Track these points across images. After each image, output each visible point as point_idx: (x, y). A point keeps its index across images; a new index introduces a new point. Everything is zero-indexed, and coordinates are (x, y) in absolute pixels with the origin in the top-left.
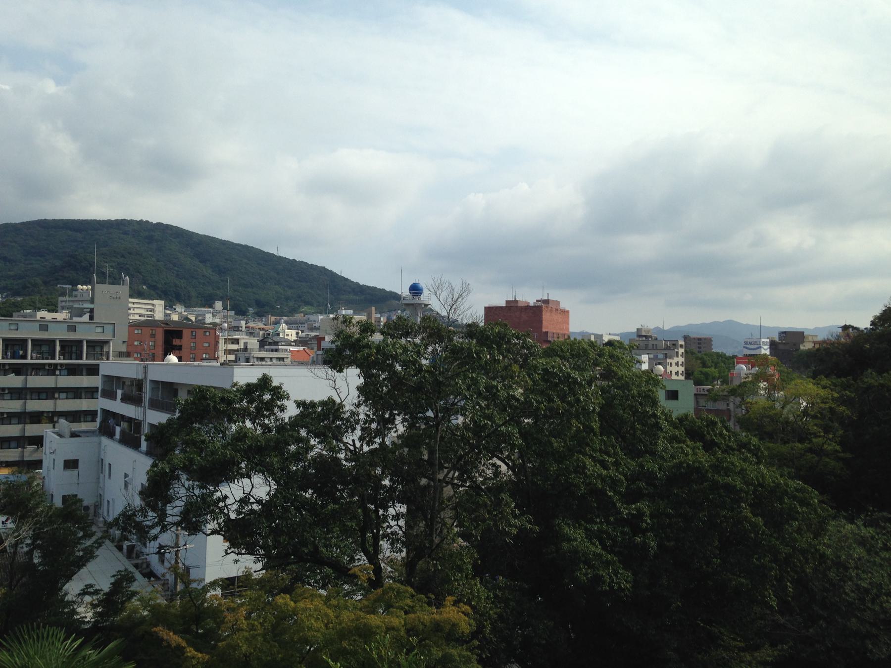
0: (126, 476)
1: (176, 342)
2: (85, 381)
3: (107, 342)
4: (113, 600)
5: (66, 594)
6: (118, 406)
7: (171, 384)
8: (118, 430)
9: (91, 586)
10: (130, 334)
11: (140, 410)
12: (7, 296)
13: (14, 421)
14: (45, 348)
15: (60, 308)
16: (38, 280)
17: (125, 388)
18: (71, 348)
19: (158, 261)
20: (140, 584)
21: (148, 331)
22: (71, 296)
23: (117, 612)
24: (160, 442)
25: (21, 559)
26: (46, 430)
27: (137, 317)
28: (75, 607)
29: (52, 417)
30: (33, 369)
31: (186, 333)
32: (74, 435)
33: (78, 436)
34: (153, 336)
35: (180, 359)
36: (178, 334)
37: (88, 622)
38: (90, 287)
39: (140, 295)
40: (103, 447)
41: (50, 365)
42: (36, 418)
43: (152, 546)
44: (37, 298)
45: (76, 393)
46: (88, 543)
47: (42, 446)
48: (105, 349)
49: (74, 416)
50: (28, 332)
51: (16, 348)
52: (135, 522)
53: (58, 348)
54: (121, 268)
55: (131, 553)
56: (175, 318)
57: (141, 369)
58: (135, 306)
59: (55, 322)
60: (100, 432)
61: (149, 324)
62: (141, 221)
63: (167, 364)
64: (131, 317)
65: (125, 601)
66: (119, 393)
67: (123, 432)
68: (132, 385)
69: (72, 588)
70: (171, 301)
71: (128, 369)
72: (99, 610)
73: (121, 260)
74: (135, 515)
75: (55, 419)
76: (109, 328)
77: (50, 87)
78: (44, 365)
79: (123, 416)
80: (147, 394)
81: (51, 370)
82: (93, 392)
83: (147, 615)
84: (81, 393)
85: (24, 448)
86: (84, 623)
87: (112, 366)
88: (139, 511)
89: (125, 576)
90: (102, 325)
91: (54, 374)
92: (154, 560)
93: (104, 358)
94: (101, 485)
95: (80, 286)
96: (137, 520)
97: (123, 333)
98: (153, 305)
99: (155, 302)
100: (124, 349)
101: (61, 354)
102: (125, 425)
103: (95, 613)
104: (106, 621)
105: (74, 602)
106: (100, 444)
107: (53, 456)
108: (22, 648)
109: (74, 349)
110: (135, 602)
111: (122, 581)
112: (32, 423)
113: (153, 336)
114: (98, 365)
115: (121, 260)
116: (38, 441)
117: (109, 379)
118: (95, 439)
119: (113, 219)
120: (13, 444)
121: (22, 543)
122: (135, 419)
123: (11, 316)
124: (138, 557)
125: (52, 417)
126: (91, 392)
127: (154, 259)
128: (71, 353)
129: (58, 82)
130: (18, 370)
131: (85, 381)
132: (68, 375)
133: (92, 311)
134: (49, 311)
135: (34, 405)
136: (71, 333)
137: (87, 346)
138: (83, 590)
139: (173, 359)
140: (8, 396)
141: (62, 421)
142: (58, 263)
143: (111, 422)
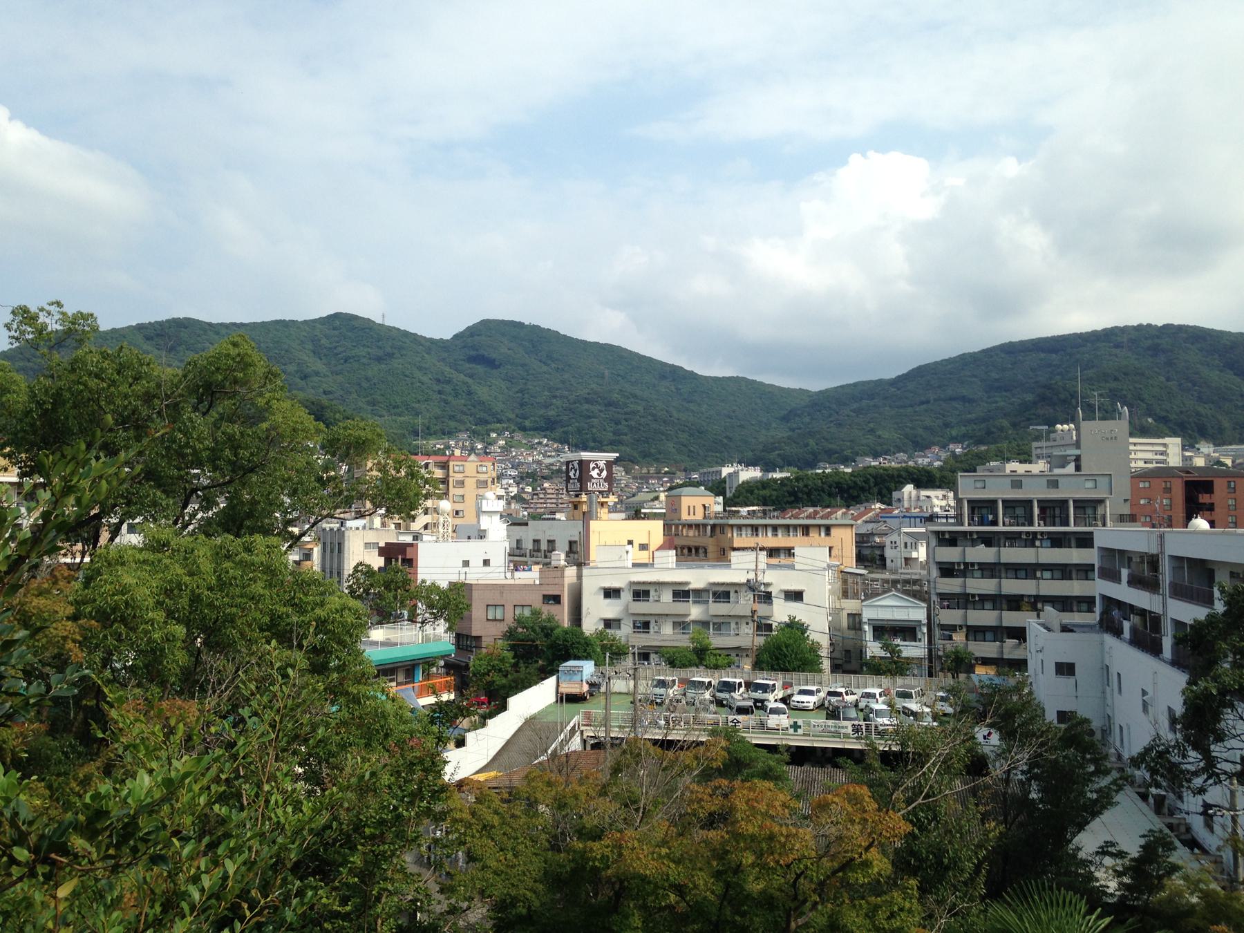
0: (1144, 693)
1: (1204, 499)
2: (1074, 556)
3: (1101, 501)
4: (1145, 869)
5: (1079, 849)
6: (1123, 592)
7: (1203, 562)
8: (1126, 625)
9: (1113, 844)
10: (1135, 490)
11: (1157, 599)
12: (968, 446)
13: (988, 605)
14: (1020, 511)
15: (1034, 458)
16: (1005, 423)
17: (1133, 565)
18: (1053, 510)
19: (1168, 380)
20: (1180, 856)
21: (1159, 484)
22: (1048, 439)
23: (1152, 889)
24: (1195, 650)
25: (1014, 789)
26: (1026, 619)
27: (1141, 464)
28: (1093, 869)
29: (1035, 603)
30: (1007, 538)
31: (1219, 485)
32: (1065, 629)
33: (1072, 631)
34: (1168, 490)
35: (1212, 524)
36: (1208, 487)
37: (1112, 895)
38: (1072, 426)
39: (1143, 431)
40: (1107, 649)
41: (1028, 533)
42: (1015, 603)
43: (1192, 803)
44: (1004, 445)
45: (1064, 571)
46: (1104, 782)
47: (1025, 641)
48: (1100, 511)
49: (1064, 603)
50: (998, 491)
51: (984, 511)
52: (1170, 762)
53: (1036, 511)
54: (1115, 395)
55: (1159, 806)
56: (1200, 462)
57: (1154, 538)
58: (1138, 448)
59: (1027, 475)
60: (1101, 627)
61: (1162, 474)
62: (1140, 326)
63: (1190, 532)
64: (1133, 465)
65: (1163, 876)
66: (1125, 573)
67: (1134, 630)
68: (1142, 562)
69: (1087, 842)
70: (1190, 437)
71: (1136, 538)
72: (1126, 880)
73: (1113, 385)
74: (1169, 752)
75: (1039, 606)
76: (1103, 482)
77: (1010, 168)
78: (1021, 533)
79: (1132, 606)
80: (1166, 575)
81: (1030, 540)
82: (1086, 571)
83: (1198, 904)
84: (1070, 572)
85: (1002, 642)
86: (1105, 893)
87: (1110, 535)
88: (1174, 747)
89: (1160, 839)
90: (1093, 477)
91: (1033, 545)
92: (1197, 823)
93: (1099, 523)
94: (1109, 702)
95: (1059, 426)
96: (1173, 760)
97: (1123, 487)
98: (1165, 445)
99: (1167, 440)
100: (1126, 510)
101: (1040, 518)
102: (1136, 619)
103: (1120, 884)
104: (1137, 899)
105: (1091, 862)
106: (1102, 644)
107: (1040, 656)
108: (1031, 909)
109: (1057, 512)
110: (1177, 881)
111: (1154, 848)
112: (1010, 609)
113: (1168, 490)
114: (1092, 533)
115: (1113, 385)
116: (1019, 634)
117: (1108, 553)
118: (1095, 637)
119: (1099, 328)
120: (989, 635)
121: (1015, 768)
122: (1150, 612)
123: (975, 471)
124: (1171, 814)
125: (1035, 603)
126: (1085, 571)
127: (1162, 379)
128: (1054, 517)
129: (1021, 157)
130: (988, 540)
131: (1074, 556)
132: (1052, 546)
133: (1078, 459)
134: (1021, 462)
135: (1012, 586)
136: (1052, 490)
137: (1075, 508)
138: (1102, 847)
139: (1201, 523)
140: (978, 574)
141: (1048, 609)
142: (1029, 397)
143: (1115, 613)
